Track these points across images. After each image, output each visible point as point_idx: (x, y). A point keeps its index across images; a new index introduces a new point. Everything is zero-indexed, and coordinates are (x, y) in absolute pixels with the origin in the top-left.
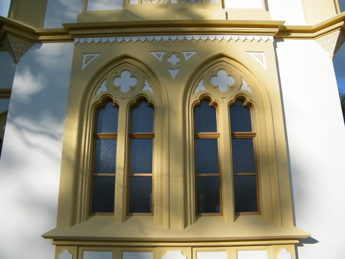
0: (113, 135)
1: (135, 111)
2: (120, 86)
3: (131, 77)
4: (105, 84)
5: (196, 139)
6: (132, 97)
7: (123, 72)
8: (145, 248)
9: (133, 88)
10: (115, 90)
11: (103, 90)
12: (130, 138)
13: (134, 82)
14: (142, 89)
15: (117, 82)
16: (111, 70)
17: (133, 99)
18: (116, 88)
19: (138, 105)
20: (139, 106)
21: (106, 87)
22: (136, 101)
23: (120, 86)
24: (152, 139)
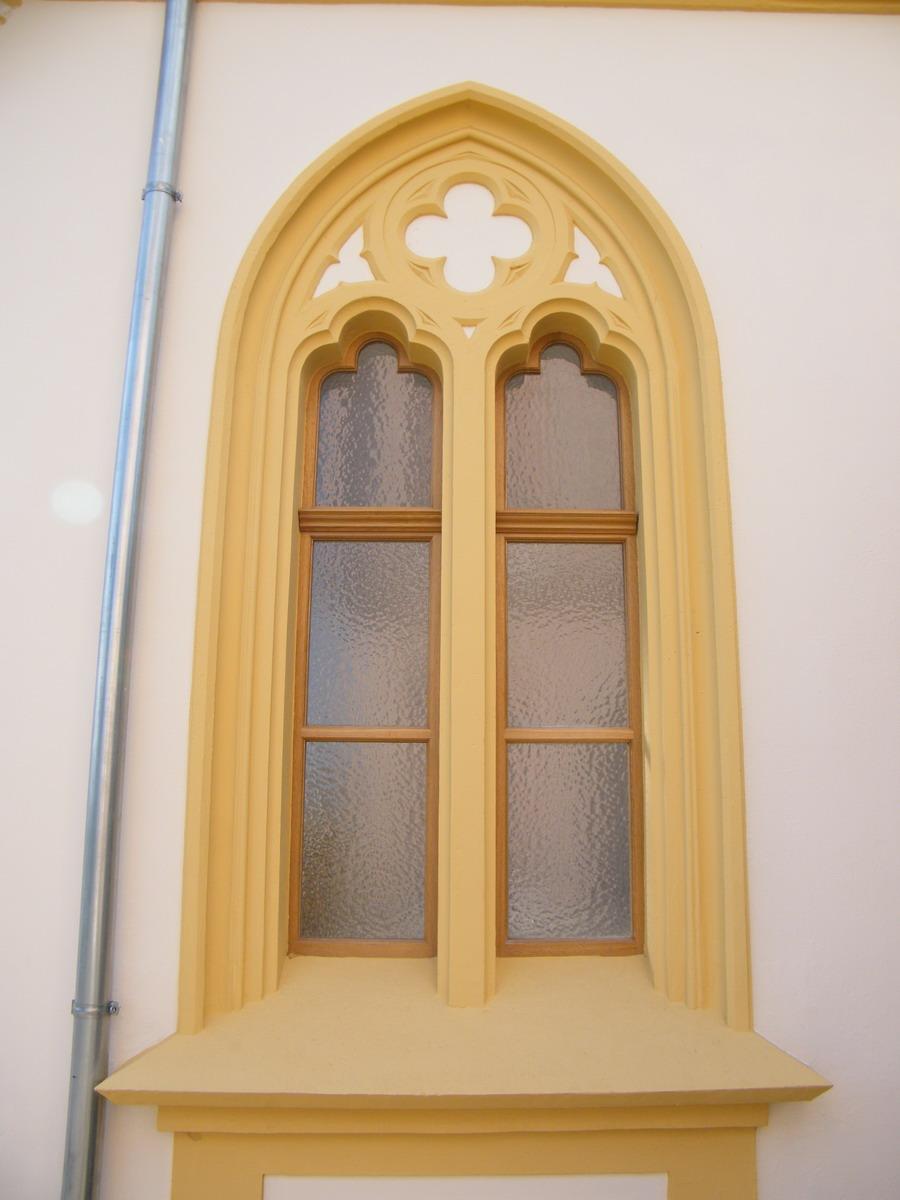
0: (606, 522)
1: (515, 393)
2: (444, 260)
3: (495, 214)
4: (333, 269)
5: (509, 541)
6: (514, 318)
7: (331, 267)
8: (106, 710)
9: (512, 269)
10: (419, 274)
11: (347, 275)
12: (307, 537)
13: (515, 239)
14: (561, 277)
15: (424, 239)
16: (337, 217)
17: (517, 326)
18: (427, 268)
19: (533, 364)
20: (536, 372)
21: (364, 264)
22: (532, 339)
23: (444, 260)
24: (428, 540)
